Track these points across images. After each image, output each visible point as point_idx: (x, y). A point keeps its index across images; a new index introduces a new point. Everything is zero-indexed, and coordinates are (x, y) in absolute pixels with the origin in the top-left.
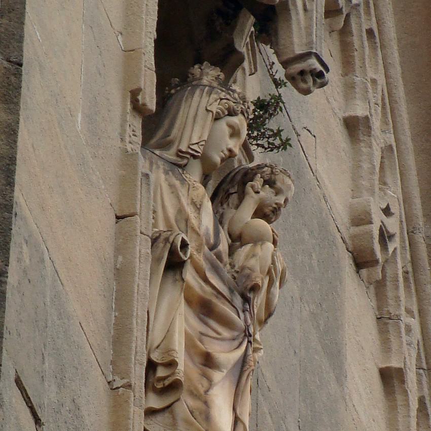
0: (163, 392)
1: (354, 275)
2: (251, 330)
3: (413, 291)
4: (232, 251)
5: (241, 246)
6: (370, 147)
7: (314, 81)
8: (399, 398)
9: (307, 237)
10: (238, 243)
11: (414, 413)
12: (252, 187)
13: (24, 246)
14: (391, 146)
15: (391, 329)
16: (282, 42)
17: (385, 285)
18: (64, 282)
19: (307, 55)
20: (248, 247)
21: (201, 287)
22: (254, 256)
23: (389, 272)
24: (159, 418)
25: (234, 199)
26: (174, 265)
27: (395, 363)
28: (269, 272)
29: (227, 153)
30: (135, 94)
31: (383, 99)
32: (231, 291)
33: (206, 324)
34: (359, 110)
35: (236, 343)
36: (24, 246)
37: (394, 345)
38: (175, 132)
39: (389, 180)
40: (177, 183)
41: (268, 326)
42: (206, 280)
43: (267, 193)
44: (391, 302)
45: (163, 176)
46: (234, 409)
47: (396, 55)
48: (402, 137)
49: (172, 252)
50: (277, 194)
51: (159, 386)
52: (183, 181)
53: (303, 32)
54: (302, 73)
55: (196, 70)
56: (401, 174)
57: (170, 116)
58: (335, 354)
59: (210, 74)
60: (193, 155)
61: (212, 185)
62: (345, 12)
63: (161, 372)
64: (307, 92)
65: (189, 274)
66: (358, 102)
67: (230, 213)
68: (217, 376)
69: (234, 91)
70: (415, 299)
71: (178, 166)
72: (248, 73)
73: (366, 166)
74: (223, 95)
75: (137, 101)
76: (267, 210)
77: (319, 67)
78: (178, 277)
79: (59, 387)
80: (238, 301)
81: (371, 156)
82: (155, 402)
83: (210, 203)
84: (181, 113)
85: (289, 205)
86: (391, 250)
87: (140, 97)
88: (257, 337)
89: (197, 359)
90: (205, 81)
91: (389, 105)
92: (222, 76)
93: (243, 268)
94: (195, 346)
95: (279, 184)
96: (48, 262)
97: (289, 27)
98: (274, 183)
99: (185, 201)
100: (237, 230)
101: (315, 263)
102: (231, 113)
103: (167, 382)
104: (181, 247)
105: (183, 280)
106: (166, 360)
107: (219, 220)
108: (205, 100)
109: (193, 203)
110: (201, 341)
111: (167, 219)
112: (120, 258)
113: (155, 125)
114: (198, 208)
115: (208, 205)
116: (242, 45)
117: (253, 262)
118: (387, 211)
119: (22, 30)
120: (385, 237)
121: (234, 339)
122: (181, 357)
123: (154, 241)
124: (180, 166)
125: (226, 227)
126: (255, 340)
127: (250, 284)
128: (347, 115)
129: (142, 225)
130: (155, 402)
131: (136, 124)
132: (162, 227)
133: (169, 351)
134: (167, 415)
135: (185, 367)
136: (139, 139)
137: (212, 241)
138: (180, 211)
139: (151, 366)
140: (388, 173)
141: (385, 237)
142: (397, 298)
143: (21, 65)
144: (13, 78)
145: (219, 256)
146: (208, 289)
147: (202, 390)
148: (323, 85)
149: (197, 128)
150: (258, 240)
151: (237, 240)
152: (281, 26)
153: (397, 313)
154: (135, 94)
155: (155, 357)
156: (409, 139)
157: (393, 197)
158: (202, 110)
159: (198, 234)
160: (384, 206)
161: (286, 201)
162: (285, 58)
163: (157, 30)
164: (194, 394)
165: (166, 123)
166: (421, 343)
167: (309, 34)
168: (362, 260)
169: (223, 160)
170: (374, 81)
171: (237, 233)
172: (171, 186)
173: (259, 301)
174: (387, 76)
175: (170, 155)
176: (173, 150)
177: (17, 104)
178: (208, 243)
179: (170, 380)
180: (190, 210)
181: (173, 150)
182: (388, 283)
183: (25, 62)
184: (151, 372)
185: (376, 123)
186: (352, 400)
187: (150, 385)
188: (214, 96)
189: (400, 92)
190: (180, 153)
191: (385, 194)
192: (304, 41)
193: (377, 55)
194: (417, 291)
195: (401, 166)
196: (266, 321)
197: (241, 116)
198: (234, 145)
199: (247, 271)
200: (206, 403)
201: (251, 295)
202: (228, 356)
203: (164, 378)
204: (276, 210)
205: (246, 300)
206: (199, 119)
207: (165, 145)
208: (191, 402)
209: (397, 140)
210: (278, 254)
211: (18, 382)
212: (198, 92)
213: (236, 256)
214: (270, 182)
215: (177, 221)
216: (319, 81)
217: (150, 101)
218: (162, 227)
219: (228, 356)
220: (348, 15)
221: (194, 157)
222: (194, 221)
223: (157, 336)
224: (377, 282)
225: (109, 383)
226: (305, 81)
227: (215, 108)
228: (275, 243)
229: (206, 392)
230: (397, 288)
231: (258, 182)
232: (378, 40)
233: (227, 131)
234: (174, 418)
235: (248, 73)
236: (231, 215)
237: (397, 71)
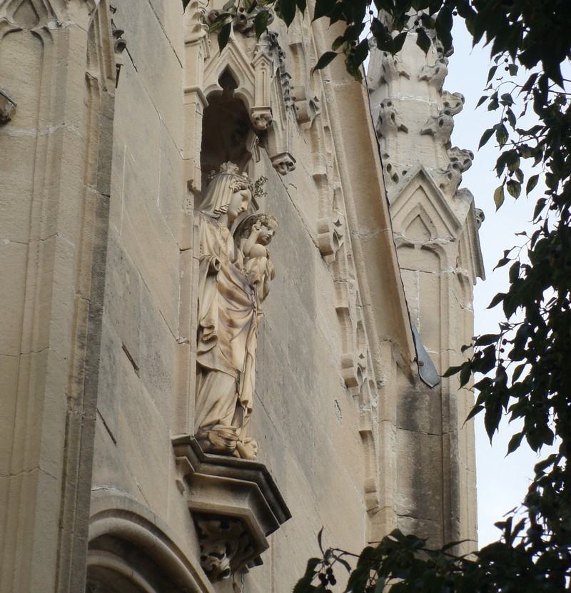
0: (207, 342)
1: (321, 260)
2: (256, 305)
3: (354, 265)
4: (245, 261)
5: (251, 258)
6: (328, 190)
7: (288, 168)
8: (347, 323)
9: (292, 243)
10: (248, 258)
11: (355, 331)
12: (255, 227)
13: (127, 275)
14: (340, 188)
15: (341, 286)
16: (270, 147)
17: (338, 263)
18: (150, 290)
19: (284, 154)
20: (253, 260)
21: (228, 284)
22: (256, 264)
23: (340, 256)
24: (205, 356)
25: (247, 232)
26: (212, 273)
27: (344, 305)
28: (265, 273)
29: (241, 210)
30: (190, 184)
31: (335, 163)
32: (244, 285)
33: (230, 303)
34: (322, 171)
35: (248, 312)
36: (127, 275)
37: (344, 295)
38: (213, 200)
39: (339, 206)
40: (214, 228)
41: (264, 302)
42: (230, 280)
43: (264, 230)
44: (341, 272)
45: (207, 225)
46: (246, 348)
47: (341, 139)
48: (346, 183)
49: (211, 267)
50: (269, 230)
51: (205, 339)
52: (217, 227)
53: (282, 142)
54: (281, 164)
55: (224, 166)
56: (346, 202)
57: (210, 192)
58: (309, 304)
59: (231, 168)
60: (222, 212)
61: (234, 227)
62: (312, 119)
63: (206, 332)
64: (284, 174)
65: (221, 277)
66: (321, 166)
67: (243, 241)
68: (236, 331)
69: (244, 177)
70: (355, 269)
71: (215, 219)
72: (255, 161)
73: (325, 200)
74: (238, 179)
75: (191, 186)
76: (264, 239)
77: (291, 161)
78: (214, 280)
79: (148, 347)
80: (248, 289)
81: (328, 195)
82: (203, 348)
83: (232, 238)
84: (216, 190)
85: (276, 235)
86: (340, 244)
87: (193, 184)
88: (260, 308)
89: (226, 323)
90: (229, 172)
91: (338, 166)
92: (238, 169)
93: (251, 271)
94: (224, 316)
95: (270, 225)
96: (141, 281)
97: (274, 139)
98: (267, 224)
99: (219, 237)
100: (248, 250)
101: (297, 257)
102: (243, 188)
103: (209, 337)
104: (216, 264)
105: (217, 281)
106: (209, 325)
107: (237, 246)
108: (229, 181)
109: (223, 238)
110: (228, 314)
111: (209, 248)
112: (183, 273)
113: (201, 197)
114: (225, 241)
115: (231, 240)
116: (252, 150)
117: (255, 268)
118: (338, 224)
119: (110, 177)
120: (336, 237)
121: (246, 311)
122: (216, 322)
123: (201, 261)
124: (216, 218)
125: (242, 249)
126: (258, 309)
127: (254, 280)
128: (314, 174)
129: (195, 252)
130: (203, 348)
131: (192, 198)
132: (207, 253)
133: (210, 320)
134: (209, 354)
135: (220, 329)
136: (192, 206)
137: (233, 258)
138: (216, 243)
139: (201, 329)
140: (338, 203)
141: (336, 237)
142: (345, 270)
143: (109, 196)
144: (105, 204)
145: (237, 266)
146: (231, 284)
147: (228, 340)
148: (293, 170)
149: (225, 197)
150: (258, 256)
151: (248, 255)
152: (270, 139)
153: (345, 278)
154: (190, 184)
155: (203, 323)
156: (350, 184)
157: (341, 215)
158: (227, 188)
159: (226, 255)
160: (336, 222)
161: (274, 233)
162: (272, 156)
163: (202, 147)
164: (224, 343)
165: (209, 194)
166: (359, 292)
167: (285, 143)
168: (324, 252)
169: (239, 214)
170: (329, 154)
171: (248, 252)
172: (211, 229)
173: (260, 289)
174: (337, 151)
175: (211, 213)
176: (212, 210)
177: (107, 217)
178: (231, 260)
179: (211, 335)
180: (221, 243)
181: (212, 210)
182: (340, 262)
183: (111, 194)
184: (201, 332)
185: (330, 177)
186: (319, 328)
187: (200, 339)
188: (234, 180)
189: (344, 159)
190: (215, 212)
191: (337, 214)
192: (282, 146)
193: (331, 140)
194: (356, 264)
195: (346, 198)
196: (264, 298)
197: (248, 190)
198: (245, 205)
199: (252, 273)
200: (230, 347)
201: (254, 286)
202: (241, 320)
203: (207, 335)
204: (269, 239)
205: (252, 288)
206: (226, 193)
207: (208, 207)
208: (222, 347)
209: (343, 184)
210: (270, 262)
211: (124, 348)
212: (225, 178)
213: (247, 265)
214: (264, 224)
215: (214, 249)
216: (290, 167)
217: (198, 185)
218: (207, 253)
219: (241, 320)
220: (314, 120)
221: (224, 213)
222: (224, 249)
223: (203, 312)
224: (333, 262)
225: (177, 340)
226: (283, 168)
227: (234, 186)
228: (268, 257)
229: (231, 341)
230: (344, 264)
231: (258, 224)
232: (331, 132)
233: (241, 197)
234: (213, 356)
235: (255, 161)
236: (244, 242)
237: (342, 148)
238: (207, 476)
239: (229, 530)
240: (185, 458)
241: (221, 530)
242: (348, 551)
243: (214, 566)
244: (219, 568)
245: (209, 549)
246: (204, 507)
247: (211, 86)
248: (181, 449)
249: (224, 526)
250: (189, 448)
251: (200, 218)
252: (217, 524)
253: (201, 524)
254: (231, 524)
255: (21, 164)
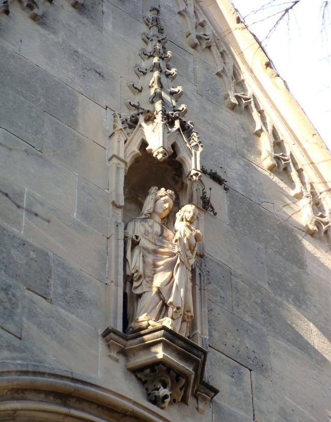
163: (124, 184)
238: (174, 344)
239: (157, 372)
240: (112, 341)
241: (152, 374)
242: (18, 339)
243: (155, 396)
244: (159, 396)
245: (151, 387)
246: (147, 361)
247: (132, 153)
248: (108, 337)
249: (153, 370)
250: (112, 334)
251: (135, 221)
252: (148, 371)
253: (139, 375)
254: (156, 368)
255: (76, 275)
